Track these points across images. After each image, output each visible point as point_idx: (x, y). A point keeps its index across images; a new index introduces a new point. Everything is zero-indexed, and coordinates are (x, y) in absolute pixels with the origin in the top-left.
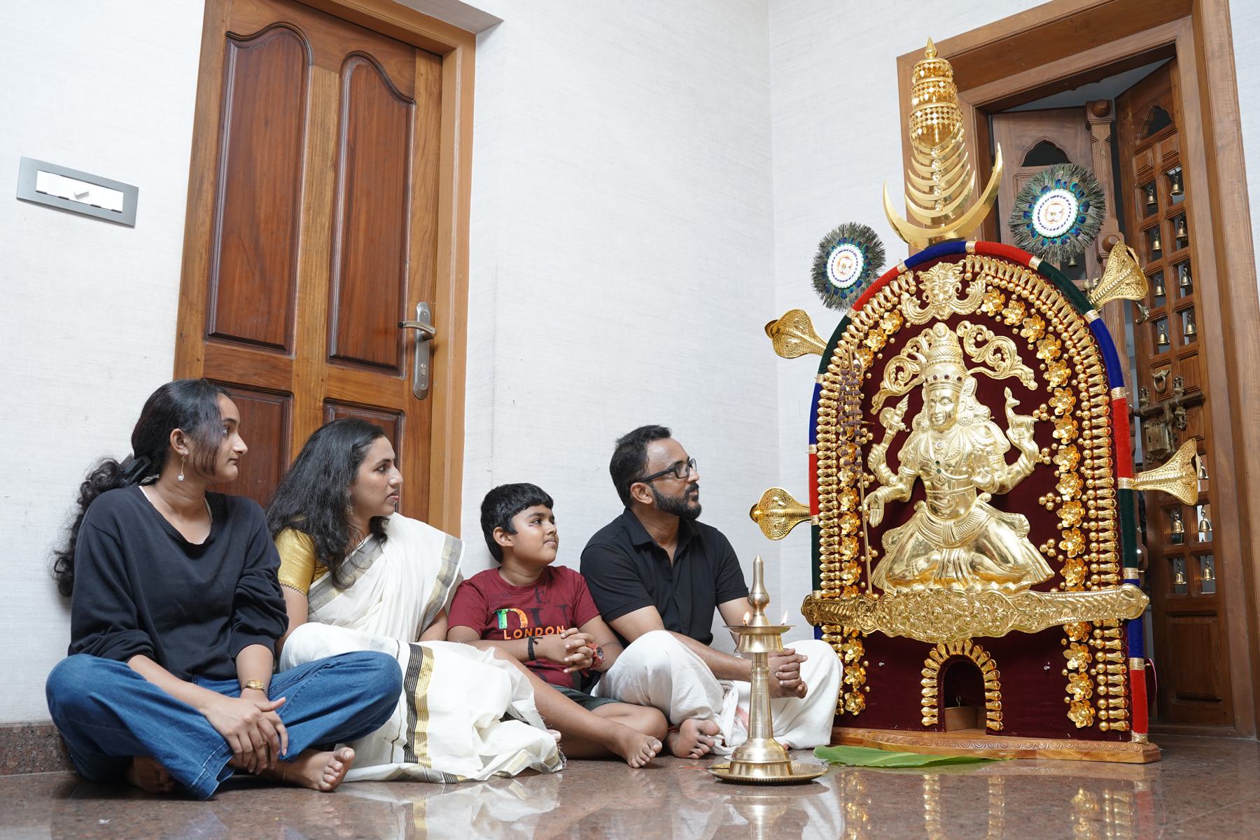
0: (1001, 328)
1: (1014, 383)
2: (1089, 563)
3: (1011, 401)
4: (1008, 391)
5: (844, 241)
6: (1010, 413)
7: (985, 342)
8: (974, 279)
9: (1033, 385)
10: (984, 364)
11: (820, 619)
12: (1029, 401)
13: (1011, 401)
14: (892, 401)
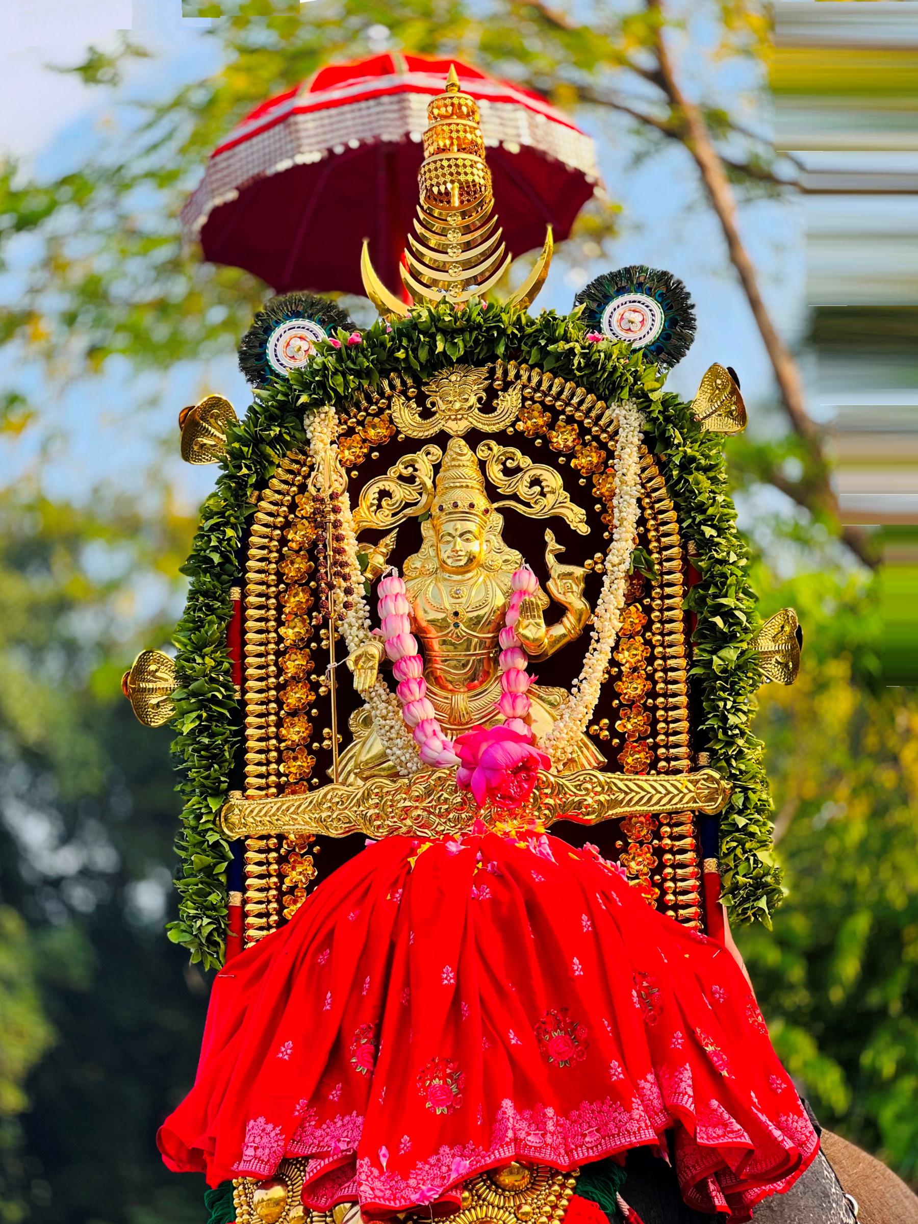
0: (544, 454)
1: (558, 524)
2: (656, 746)
4: (549, 536)
6: (550, 559)
7: (518, 469)
8: (505, 389)
9: (584, 529)
12: (577, 549)
14: (369, 536)
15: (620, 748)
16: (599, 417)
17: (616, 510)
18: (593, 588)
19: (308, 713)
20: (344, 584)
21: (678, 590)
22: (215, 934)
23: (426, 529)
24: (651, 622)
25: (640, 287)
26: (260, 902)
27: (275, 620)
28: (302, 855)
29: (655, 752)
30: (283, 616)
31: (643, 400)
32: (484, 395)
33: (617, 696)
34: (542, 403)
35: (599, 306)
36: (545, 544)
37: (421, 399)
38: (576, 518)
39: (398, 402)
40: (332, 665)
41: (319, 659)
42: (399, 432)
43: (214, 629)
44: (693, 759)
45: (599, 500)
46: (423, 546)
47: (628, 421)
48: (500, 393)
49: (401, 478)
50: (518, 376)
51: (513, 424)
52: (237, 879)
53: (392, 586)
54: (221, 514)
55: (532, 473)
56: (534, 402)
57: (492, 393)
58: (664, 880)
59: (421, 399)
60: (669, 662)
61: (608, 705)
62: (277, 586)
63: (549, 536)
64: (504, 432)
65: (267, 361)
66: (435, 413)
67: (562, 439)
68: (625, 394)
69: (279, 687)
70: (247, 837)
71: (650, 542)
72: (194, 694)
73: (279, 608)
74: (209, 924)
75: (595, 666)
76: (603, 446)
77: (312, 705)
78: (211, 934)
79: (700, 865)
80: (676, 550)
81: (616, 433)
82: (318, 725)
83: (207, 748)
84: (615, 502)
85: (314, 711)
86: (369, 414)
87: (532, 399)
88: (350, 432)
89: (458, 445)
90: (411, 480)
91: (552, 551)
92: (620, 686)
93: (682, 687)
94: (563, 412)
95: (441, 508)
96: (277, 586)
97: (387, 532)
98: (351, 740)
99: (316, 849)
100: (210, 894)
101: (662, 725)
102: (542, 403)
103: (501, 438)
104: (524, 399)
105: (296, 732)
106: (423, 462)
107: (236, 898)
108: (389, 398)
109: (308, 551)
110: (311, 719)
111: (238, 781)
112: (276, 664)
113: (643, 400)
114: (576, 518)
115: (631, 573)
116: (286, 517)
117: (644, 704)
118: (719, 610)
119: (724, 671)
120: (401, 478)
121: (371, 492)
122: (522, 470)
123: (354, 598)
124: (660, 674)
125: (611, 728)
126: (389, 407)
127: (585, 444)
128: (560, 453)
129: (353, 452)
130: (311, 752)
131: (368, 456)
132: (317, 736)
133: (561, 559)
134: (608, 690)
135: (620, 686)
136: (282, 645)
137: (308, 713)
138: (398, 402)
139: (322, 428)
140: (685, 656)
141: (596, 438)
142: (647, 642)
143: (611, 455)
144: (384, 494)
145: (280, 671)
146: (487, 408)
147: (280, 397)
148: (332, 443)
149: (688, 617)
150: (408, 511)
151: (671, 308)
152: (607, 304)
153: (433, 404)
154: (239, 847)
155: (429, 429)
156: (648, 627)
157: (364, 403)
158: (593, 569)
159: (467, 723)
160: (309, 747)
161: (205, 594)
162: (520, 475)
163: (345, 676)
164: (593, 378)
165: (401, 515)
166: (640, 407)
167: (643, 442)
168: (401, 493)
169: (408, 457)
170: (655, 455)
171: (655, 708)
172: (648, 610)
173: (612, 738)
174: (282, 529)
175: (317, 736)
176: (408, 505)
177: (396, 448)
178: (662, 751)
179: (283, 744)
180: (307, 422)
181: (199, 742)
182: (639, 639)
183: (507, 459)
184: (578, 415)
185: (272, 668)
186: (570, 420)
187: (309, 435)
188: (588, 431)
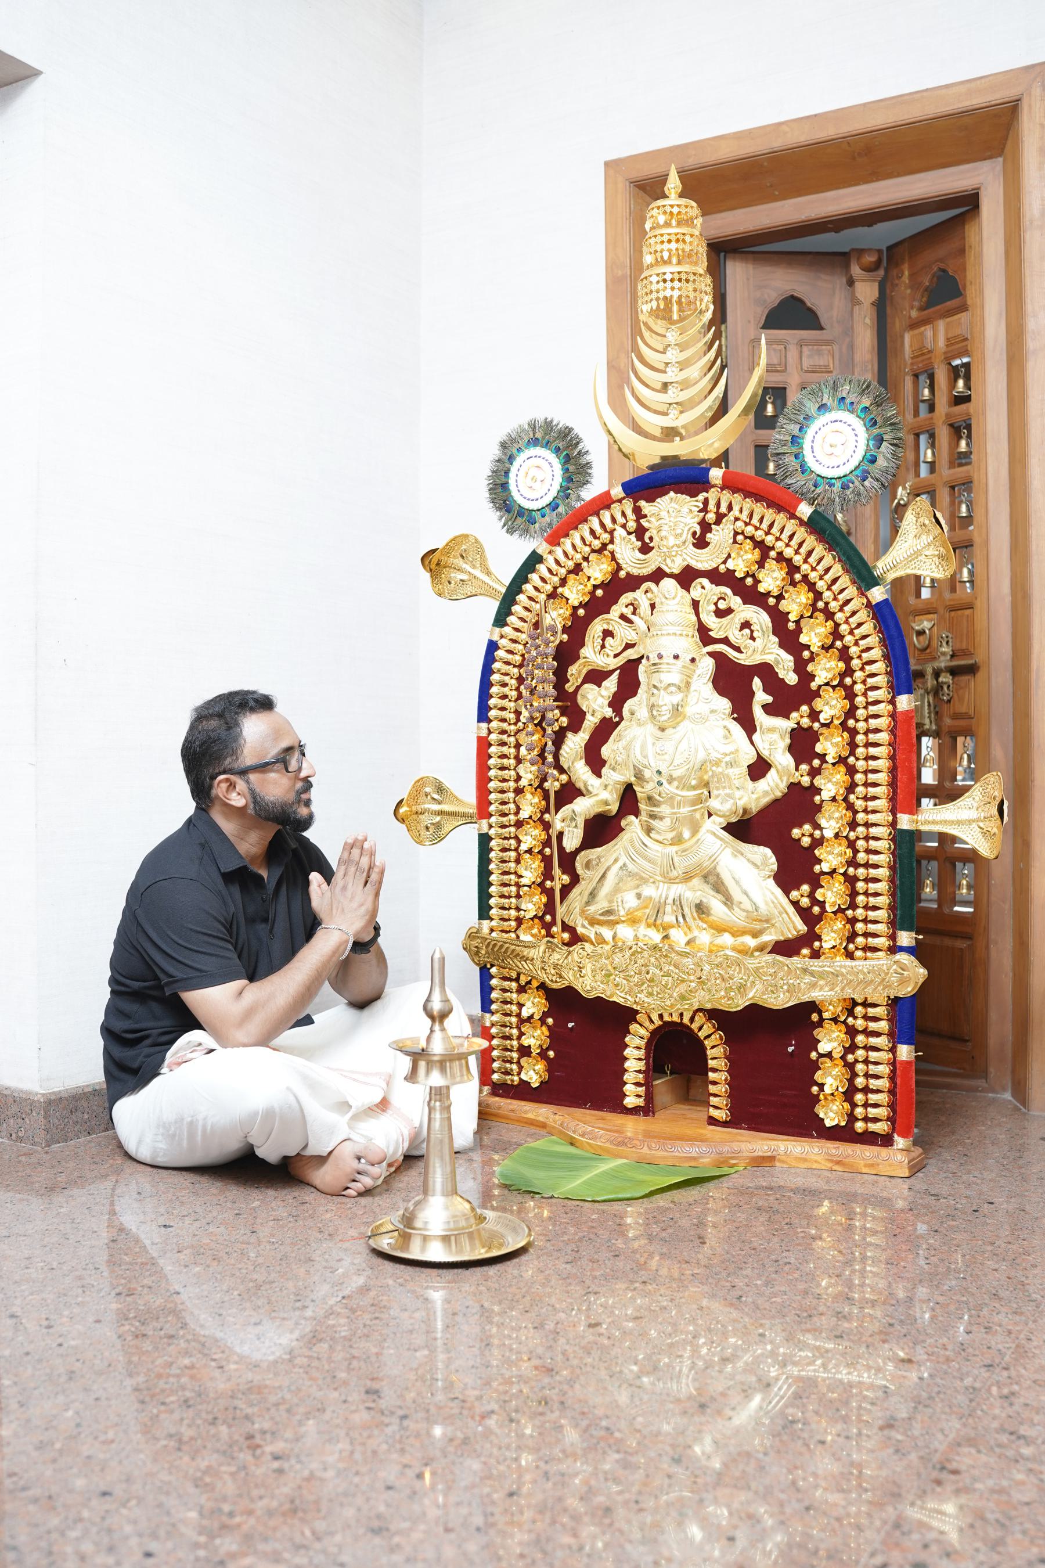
1: (766, 671)
3: (761, 697)
4: (757, 683)
5: (534, 442)
6: (758, 713)
7: (729, 611)
8: (718, 522)
9: (792, 679)
10: (726, 641)
13: (761, 697)
14: (596, 677)
57: (706, 527)
63: (757, 683)
66: (653, 548)
79: (893, 1050)
173: (812, 905)
188: (798, 569)
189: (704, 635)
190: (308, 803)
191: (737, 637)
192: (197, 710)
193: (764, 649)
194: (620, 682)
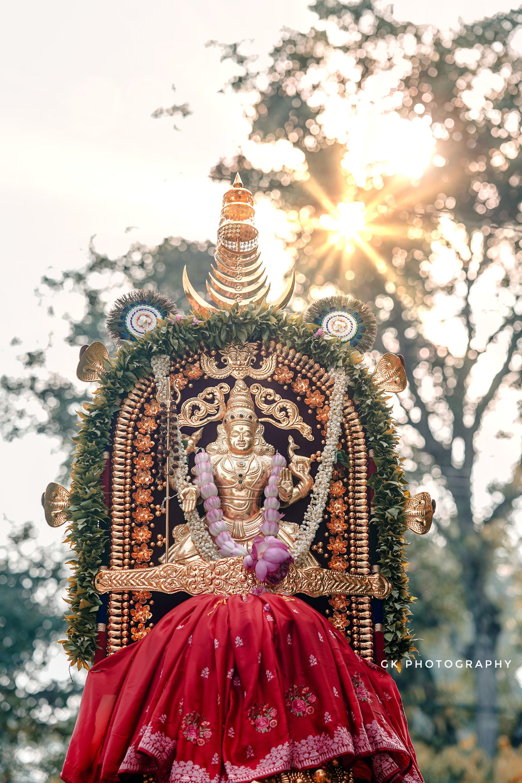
0: (289, 393)
1: (295, 433)
2: (349, 560)
3: (292, 445)
4: (291, 440)
5: (133, 251)
6: (291, 453)
7: (274, 401)
8: (267, 357)
9: (311, 438)
10: (271, 416)
11: (346, 294)
12: (307, 448)
13: (292, 445)
14: (188, 431)
15: (329, 559)
16: (321, 377)
17: (328, 429)
18: (313, 472)
19: (149, 526)
20: (174, 455)
21: (363, 475)
22: (90, 648)
23: (221, 429)
24: (348, 492)
25: (344, 308)
26: (117, 630)
27: (130, 472)
28: (143, 605)
29: (349, 562)
30: (135, 470)
31: (349, 368)
32: (255, 359)
33: (328, 530)
34: (289, 366)
35: (320, 316)
36: (288, 443)
37: (218, 357)
38: (306, 431)
39: (205, 358)
40: (167, 498)
41: (158, 497)
42: (205, 374)
43: (97, 473)
44: (371, 568)
45: (320, 423)
46: (219, 438)
47: (339, 380)
48: (264, 358)
49: (205, 399)
50: (275, 350)
51: (272, 376)
52: (103, 616)
53: (201, 457)
54: (101, 409)
55: (281, 404)
56: (284, 365)
57: (259, 357)
58: (353, 633)
59: (218, 357)
60: (357, 514)
61: (323, 534)
62: (132, 453)
63: (291, 440)
64: (266, 380)
65: (126, 327)
66: (226, 365)
67: (302, 386)
68: (340, 363)
69: (132, 510)
70: (111, 592)
71: (348, 448)
72: (83, 508)
73: (133, 466)
74: (88, 640)
75: (314, 514)
76: (323, 393)
77: (151, 522)
78: (87, 647)
79: (373, 627)
80: (363, 453)
81: (332, 386)
82: (155, 532)
83: (90, 539)
84: (328, 424)
85: (152, 525)
86: (188, 362)
87: (283, 363)
88: (177, 371)
89: (240, 384)
90: (211, 401)
91: (291, 448)
92: (330, 526)
93: (364, 528)
94: (300, 372)
95: (232, 417)
96: (132, 453)
97: (197, 429)
98: (174, 542)
99: (152, 602)
100: (86, 624)
101: (352, 548)
102: (289, 366)
103: (264, 383)
104: (278, 363)
105: (143, 535)
106: (217, 392)
107: (101, 627)
108: (200, 355)
109: (150, 435)
110: (150, 529)
111: (107, 562)
112: (130, 496)
113: (349, 368)
114: (306, 431)
115: (336, 462)
116: (137, 415)
117: (343, 536)
118: (388, 487)
119: (391, 520)
120: (205, 399)
121: (187, 406)
122: (276, 402)
123: (181, 463)
124: (352, 520)
125: (324, 548)
126: (199, 360)
127: (312, 391)
128: (298, 394)
129: (179, 382)
130: (149, 547)
131: (187, 386)
132: (154, 538)
133: (296, 452)
134: (323, 527)
135: (330, 526)
136: (134, 486)
137: (149, 526)
138: (205, 358)
139: (160, 367)
140: (367, 512)
141: (319, 388)
142: (346, 503)
143: (327, 398)
144: (195, 408)
145: (133, 501)
146: (257, 366)
147: (139, 346)
148: (167, 376)
149: (369, 491)
150: (209, 418)
151: (362, 321)
152: (325, 315)
153: (225, 360)
154: (106, 598)
155: (222, 374)
156: (346, 494)
157: (185, 357)
158: (315, 460)
159: (243, 537)
160: (148, 544)
161: (90, 453)
162: (274, 404)
163: (175, 504)
164: (322, 355)
165: (206, 420)
166: (347, 372)
167: (347, 392)
168: (204, 407)
169: (209, 389)
170: (352, 401)
171: (349, 539)
172: (346, 485)
173: (324, 553)
174: (135, 421)
175: (154, 538)
176: (209, 415)
177: (202, 383)
178: (352, 562)
179: (133, 542)
180: (153, 362)
181: (85, 536)
182: (341, 501)
183: (267, 395)
184: (309, 374)
185: (128, 499)
186: (304, 377)
187: (154, 370)
188: (315, 384)
189: (258, 412)
190: (293, 31)
191: (280, 415)
192: (261, 171)
193: (294, 421)
194: (203, 433)
